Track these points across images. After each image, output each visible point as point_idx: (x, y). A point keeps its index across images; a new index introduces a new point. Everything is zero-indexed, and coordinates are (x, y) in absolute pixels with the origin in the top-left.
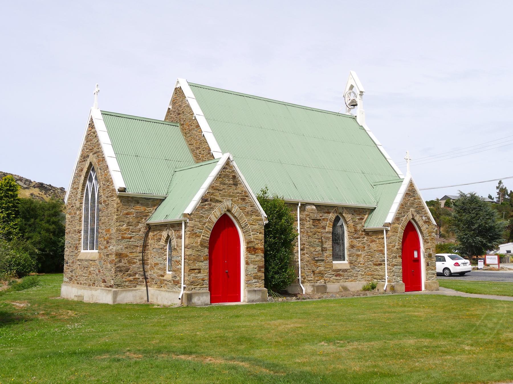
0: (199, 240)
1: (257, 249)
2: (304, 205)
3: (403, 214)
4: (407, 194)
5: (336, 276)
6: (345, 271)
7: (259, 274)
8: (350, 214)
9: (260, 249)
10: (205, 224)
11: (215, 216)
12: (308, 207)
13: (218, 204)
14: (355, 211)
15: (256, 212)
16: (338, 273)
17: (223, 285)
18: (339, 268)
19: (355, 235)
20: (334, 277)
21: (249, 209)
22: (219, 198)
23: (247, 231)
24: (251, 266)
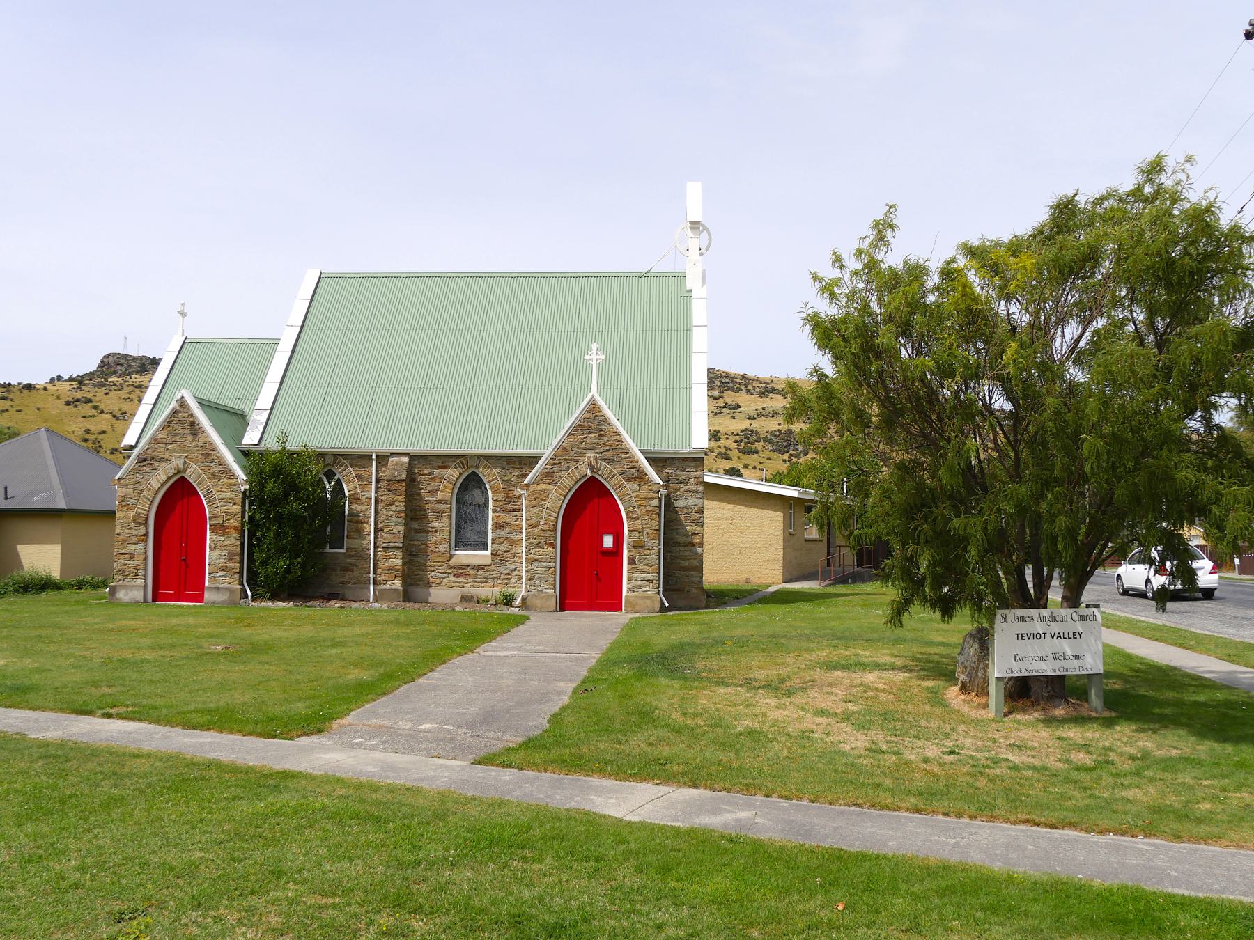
0: (132, 513)
1: (227, 528)
2: (383, 458)
3: (563, 466)
4: (579, 426)
5: (457, 576)
6: (482, 567)
7: (230, 564)
8: (496, 467)
9: (234, 528)
10: (142, 491)
11: (159, 480)
12: (392, 460)
13: (163, 464)
14: (508, 463)
15: (229, 473)
16: (461, 571)
17: (177, 574)
18: (465, 562)
19: (506, 507)
20: (452, 578)
21: (217, 468)
22: (166, 456)
23: (933, 498)
24: (217, 553)
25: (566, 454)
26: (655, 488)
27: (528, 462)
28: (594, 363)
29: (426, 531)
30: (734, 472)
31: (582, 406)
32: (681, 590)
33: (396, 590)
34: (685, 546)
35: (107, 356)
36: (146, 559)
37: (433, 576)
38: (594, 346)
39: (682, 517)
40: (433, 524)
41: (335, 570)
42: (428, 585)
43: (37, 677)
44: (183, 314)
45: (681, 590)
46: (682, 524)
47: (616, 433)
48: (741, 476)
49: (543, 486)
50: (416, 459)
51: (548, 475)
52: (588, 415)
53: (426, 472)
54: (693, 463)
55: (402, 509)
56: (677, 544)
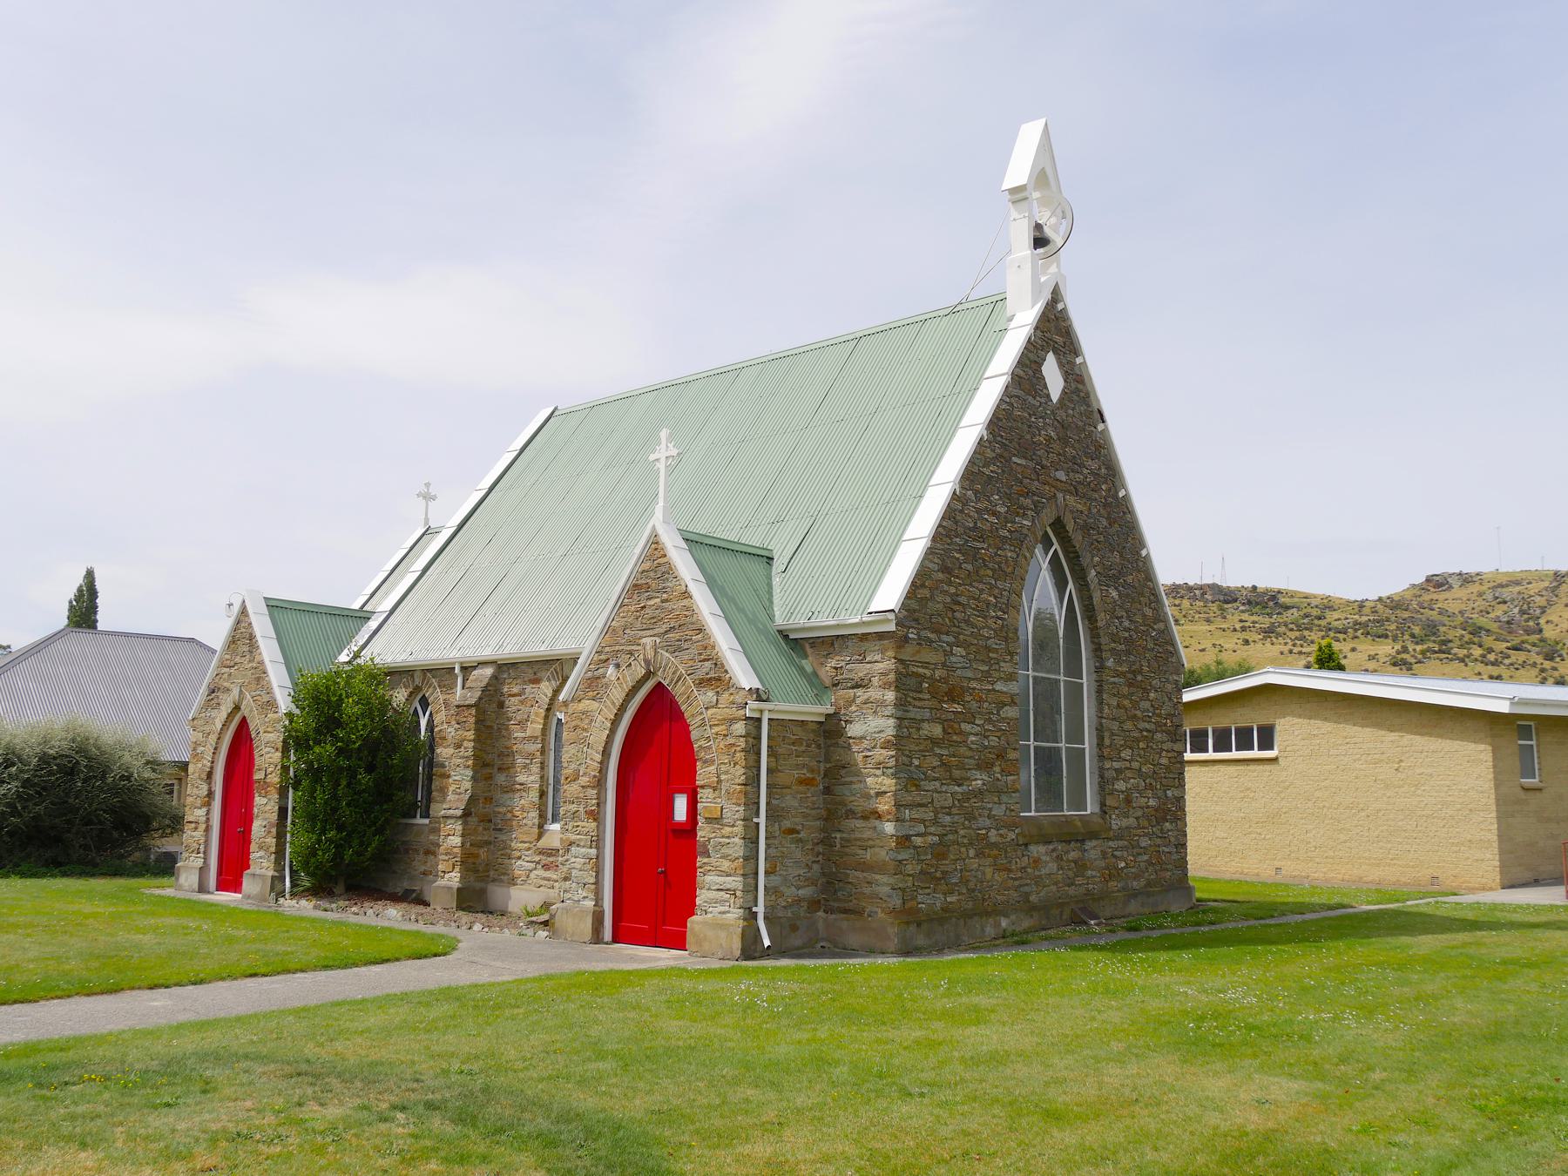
2: (466, 669)
5: (546, 867)
20: (541, 872)
25: (612, 647)
26: (739, 698)
27: (557, 666)
28: (661, 466)
29: (510, 789)
30: (1328, 661)
31: (638, 551)
32: (859, 913)
33: (450, 888)
34: (865, 818)
35: (1437, 583)
36: (208, 829)
37: (520, 866)
38: (664, 434)
39: (859, 757)
40: (521, 778)
41: (416, 851)
42: (513, 882)
43: (1429, 988)
44: (428, 497)
45: (859, 913)
46: (858, 773)
47: (686, 594)
48: (1341, 668)
49: (586, 704)
50: (505, 669)
51: (593, 683)
52: (647, 566)
53: (515, 690)
54: (878, 645)
55: (470, 753)
56: (851, 814)
